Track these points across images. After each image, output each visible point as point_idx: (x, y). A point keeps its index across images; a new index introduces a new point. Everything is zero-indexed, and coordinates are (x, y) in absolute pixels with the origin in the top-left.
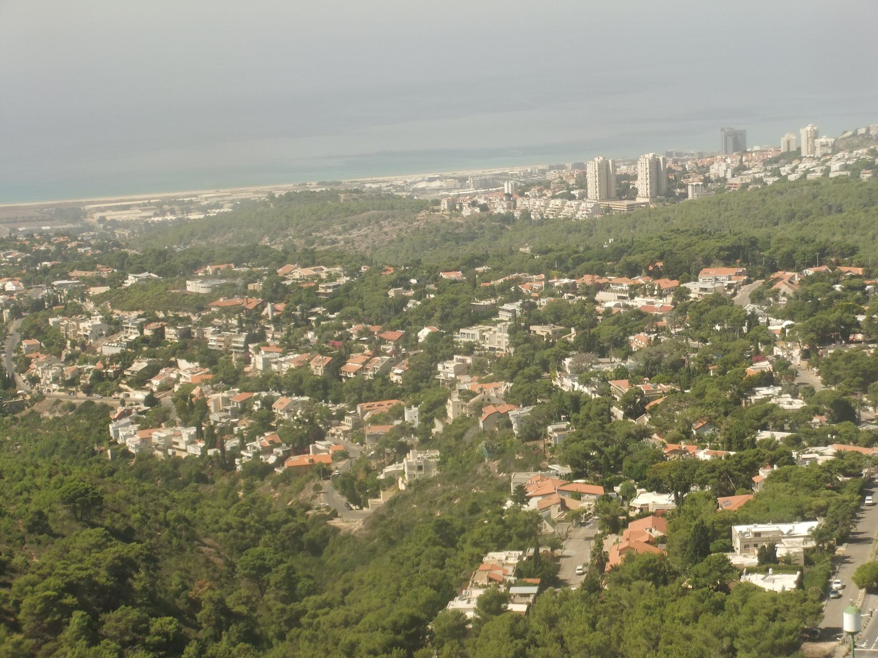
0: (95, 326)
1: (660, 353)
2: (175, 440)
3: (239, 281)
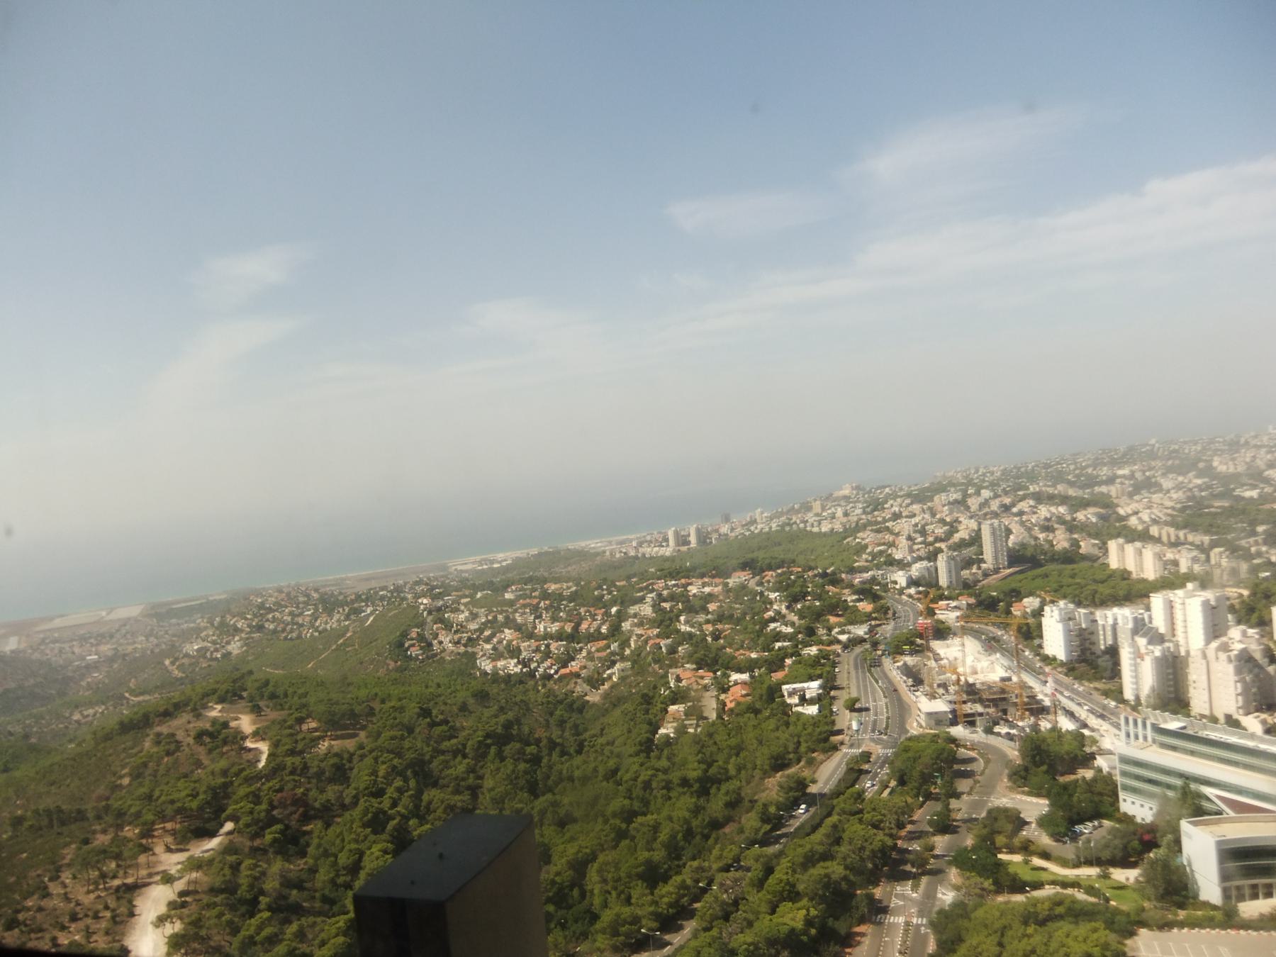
1: (723, 612)
3: (528, 592)
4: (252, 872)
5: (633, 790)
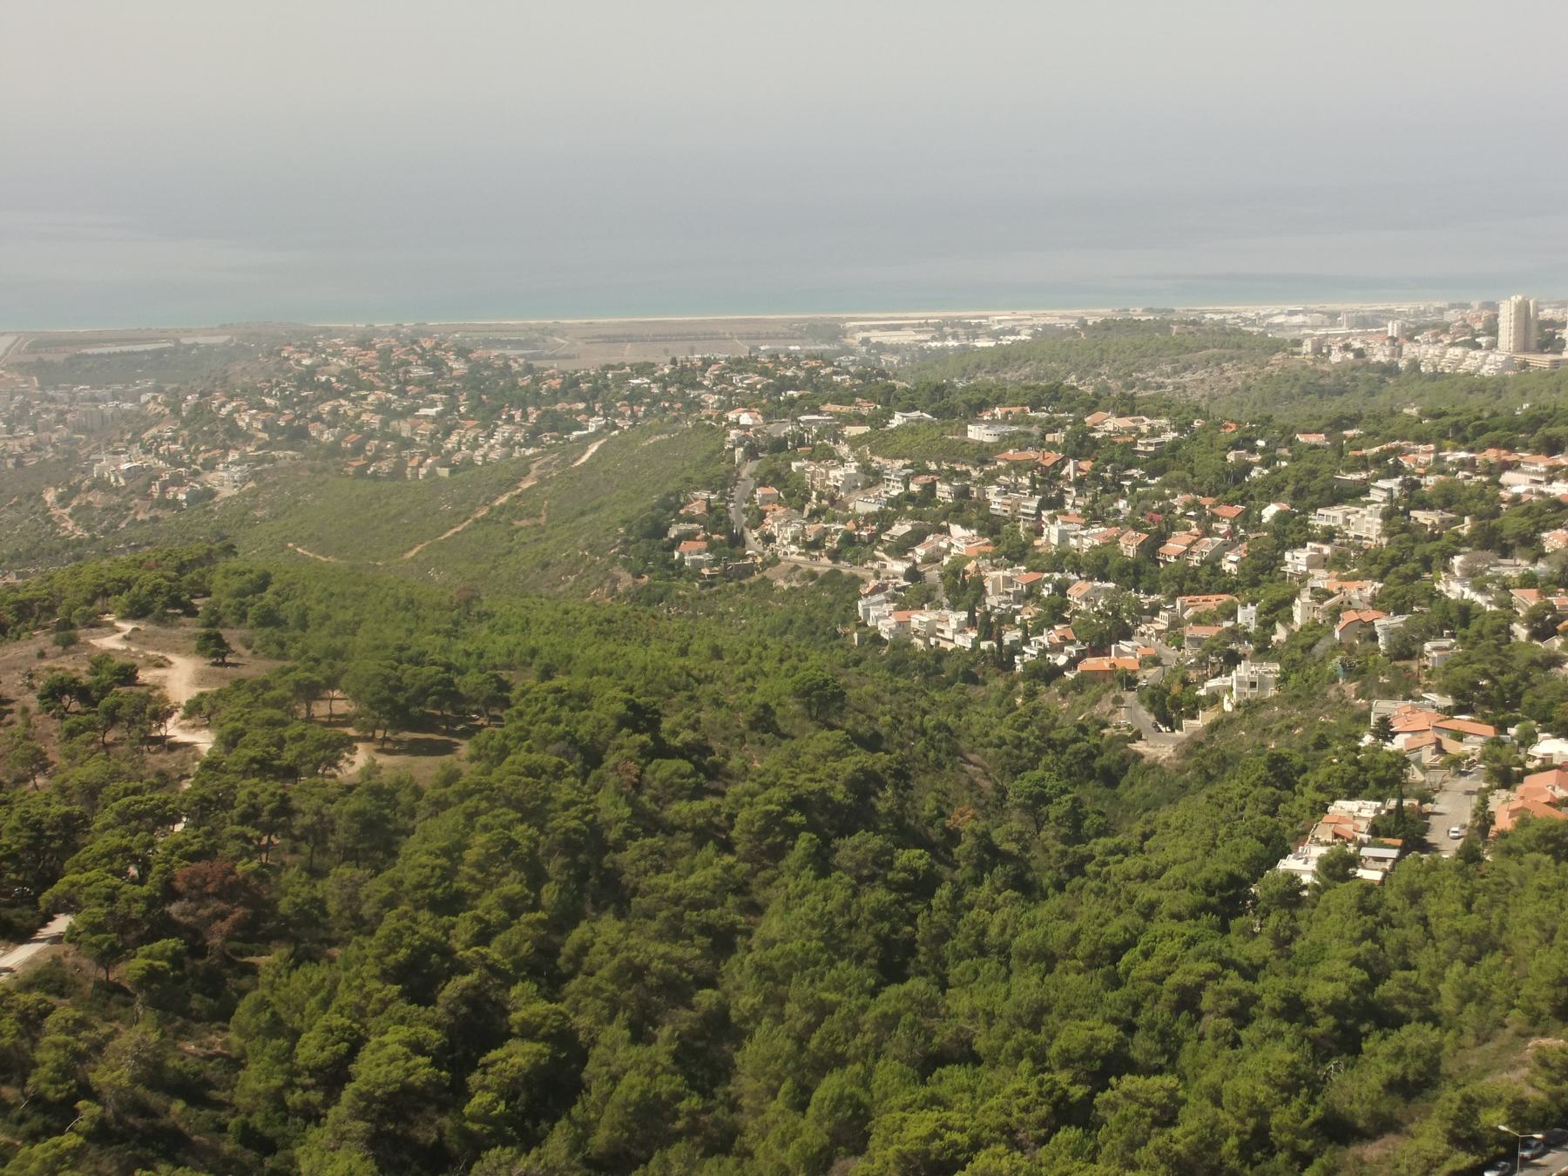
2: (939, 626)
3: (1035, 430)
4: (71, 1038)
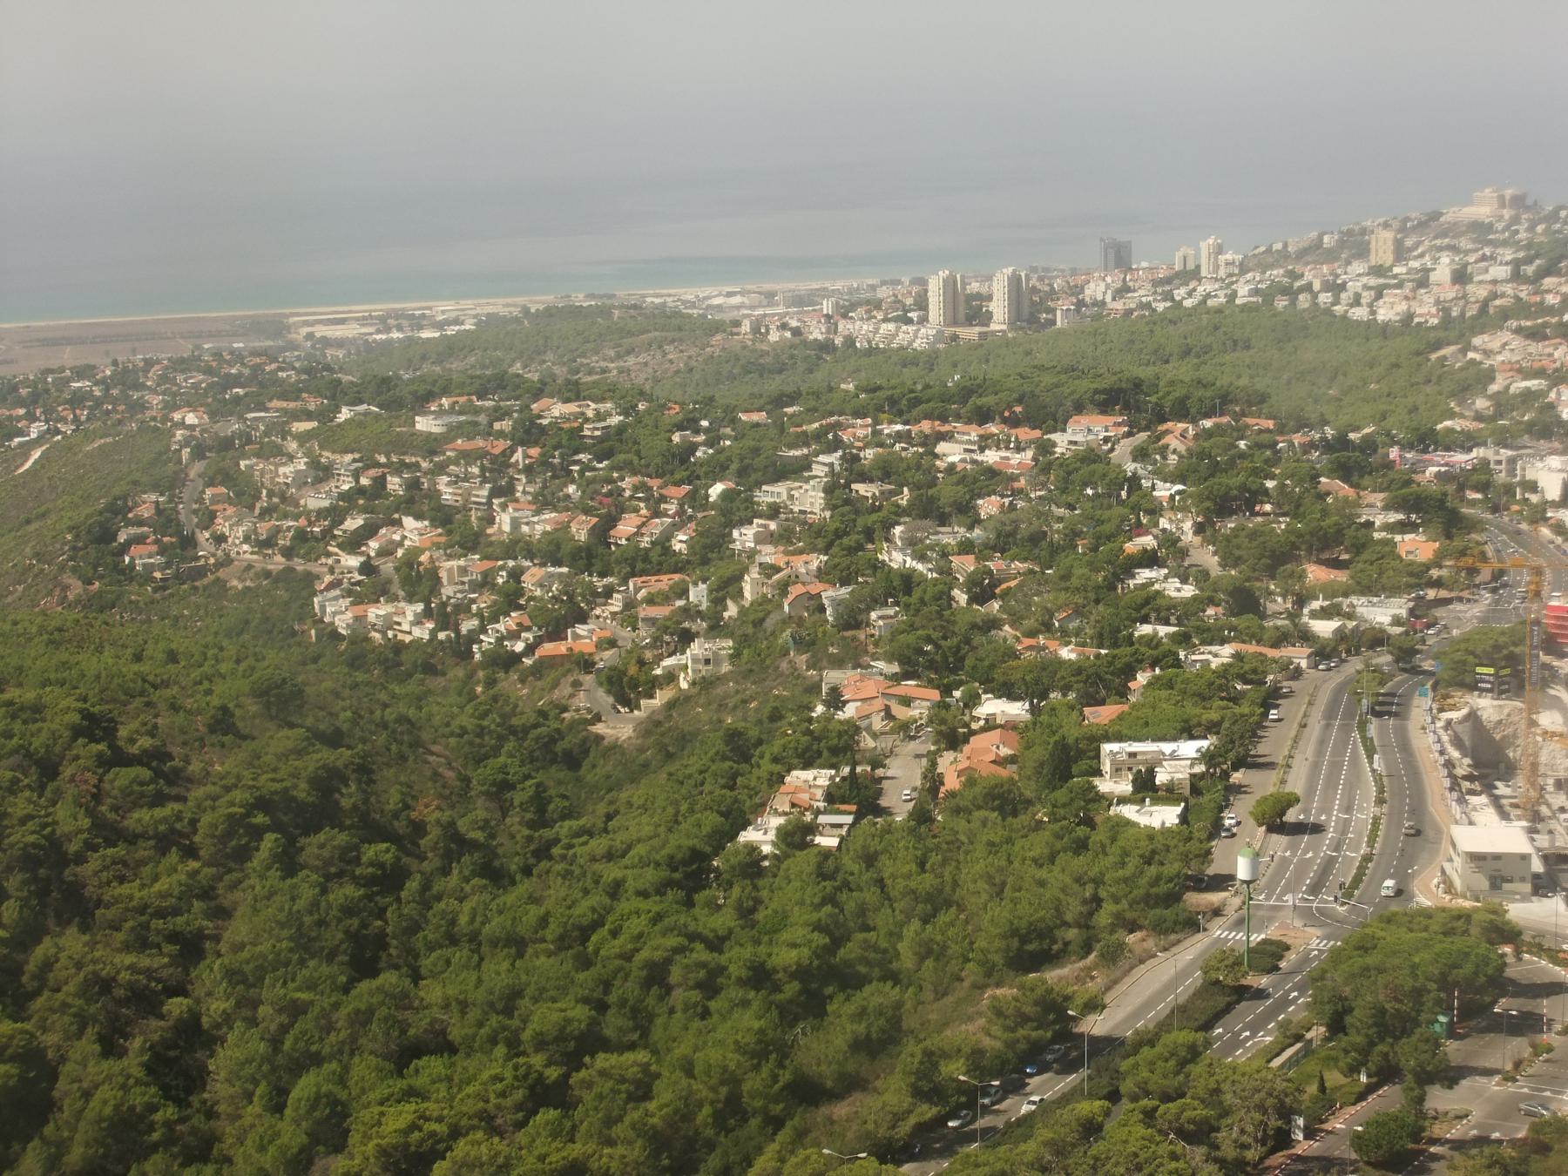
0: (298, 472)
2: (396, 619)
3: (483, 419)
5: (617, 983)
